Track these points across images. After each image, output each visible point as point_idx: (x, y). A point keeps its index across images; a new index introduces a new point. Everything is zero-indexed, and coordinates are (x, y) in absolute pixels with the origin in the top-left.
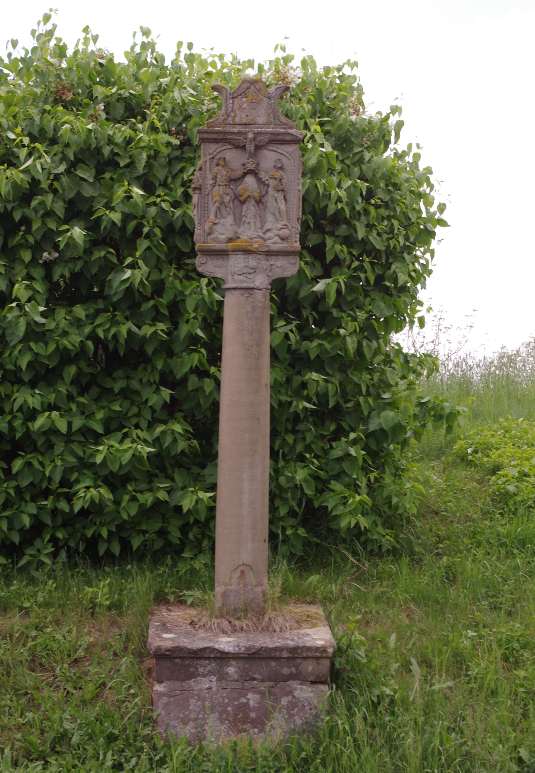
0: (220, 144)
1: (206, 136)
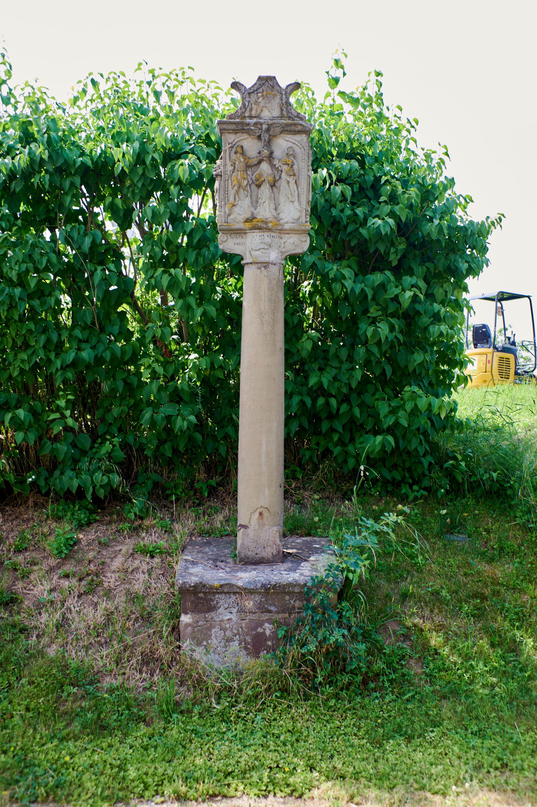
0: (238, 135)
1: (225, 126)
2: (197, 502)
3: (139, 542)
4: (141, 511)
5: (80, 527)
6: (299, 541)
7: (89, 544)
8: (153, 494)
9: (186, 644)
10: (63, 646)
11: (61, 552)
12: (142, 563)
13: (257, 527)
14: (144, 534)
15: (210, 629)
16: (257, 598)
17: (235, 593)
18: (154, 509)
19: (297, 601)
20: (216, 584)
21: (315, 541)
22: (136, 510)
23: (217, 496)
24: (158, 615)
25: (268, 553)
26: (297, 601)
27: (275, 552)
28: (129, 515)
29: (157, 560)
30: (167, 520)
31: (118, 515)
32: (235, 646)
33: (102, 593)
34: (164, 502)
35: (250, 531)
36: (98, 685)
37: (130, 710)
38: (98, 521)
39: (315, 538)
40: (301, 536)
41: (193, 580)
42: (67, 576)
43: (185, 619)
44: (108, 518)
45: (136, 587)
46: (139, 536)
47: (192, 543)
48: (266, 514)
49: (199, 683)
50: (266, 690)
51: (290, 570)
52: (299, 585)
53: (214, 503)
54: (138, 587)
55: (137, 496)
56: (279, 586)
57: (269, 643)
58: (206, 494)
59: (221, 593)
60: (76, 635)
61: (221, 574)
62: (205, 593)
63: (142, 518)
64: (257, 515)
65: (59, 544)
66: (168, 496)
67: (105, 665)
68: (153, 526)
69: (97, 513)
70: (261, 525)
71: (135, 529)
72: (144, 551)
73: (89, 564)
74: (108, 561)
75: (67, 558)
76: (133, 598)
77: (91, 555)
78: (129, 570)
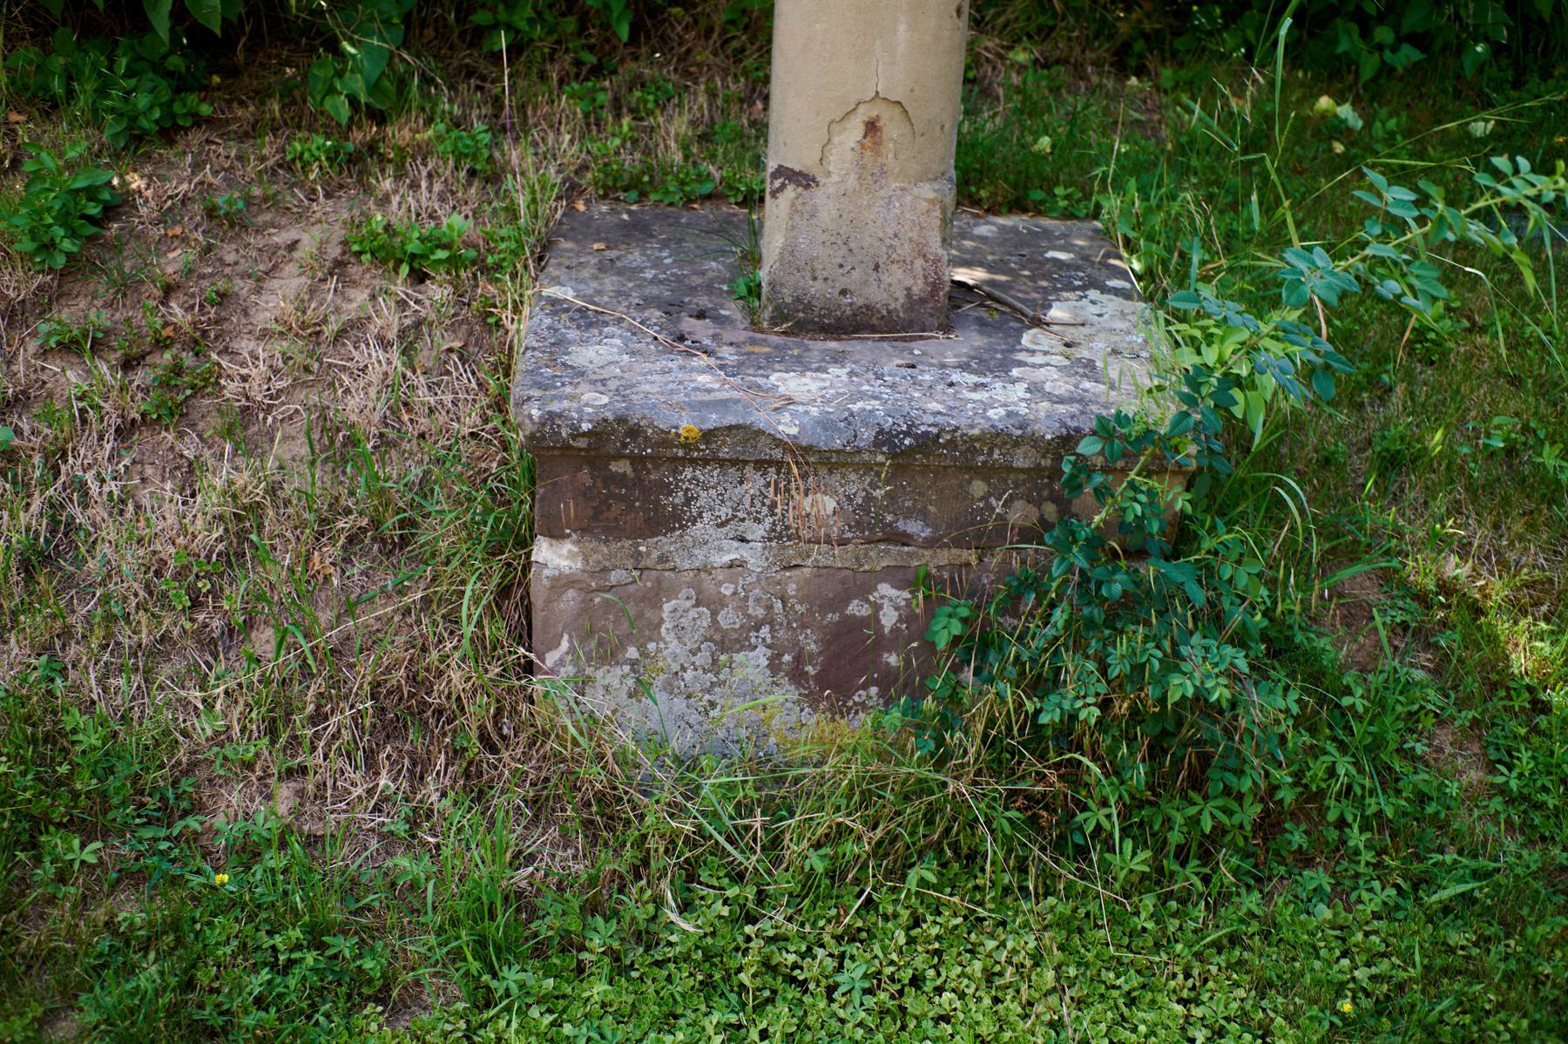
2: (591, 59)
3: (368, 217)
4: (374, 88)
5: (135, 144)
6: (984, 230)
7: (165, 217)
8: (423, 25)
9: (557, 656)
10: (47, 648)
11: (49, 247)
12: (378, 302)
13: (852, 181)
14: (387, 184)
15: (653, 599)
16: (855, 485)
17: (761, 465)
18: (426, 80)
19: (1019, 504)
20: (687, 425)
21: (1046, 233)
22: (358, 84)
23: (664, 39)
24: (441, 530)
25: (892, 288)
26: (1019, 504)
27: (919, 288)
28: (328, 105)
29: (438, 291)
30: (479, 126)
31: (291, 98)
32: (753, 663)
33: (214, 422)
34: (464, 57)
35: (824, 200)
36: (193, 823)
37: (321, 947)
38: (209, 121)
39: (1046, 222)
40: (993, 210)
41: (588, 404)
42: (69, 347)
43: (553, 557)
44: (246, 113)
45: (353, 403)
46: (368, 190)
47: (582, 230)
48: (893, 129)
49: (606, 816)
50: (880, 850)
51: (981, 364)
52: (1035, 441)
53: (654, 67)
54: (360, 406)
55: (358, 31)
56: (952, 444)
57: (893, 659)
58: (624, 32)
59: (706, 462)
60: (105, 600)
61: (705, 379)
62: (637, 461)
63: (380, 118)
64: (854, 132)
65: (38, 213)
66: (478, 36)
67: (220, 738)
68: (424, 151)
69: (205, 90)
70: (872, 175)
71: (354, 159)
72: (387, 254)
73: (164, 301)
74: (243, 287)
75: (75, 269)
76: (338, 445)
77: (174, 261)
78: (329, 330)
